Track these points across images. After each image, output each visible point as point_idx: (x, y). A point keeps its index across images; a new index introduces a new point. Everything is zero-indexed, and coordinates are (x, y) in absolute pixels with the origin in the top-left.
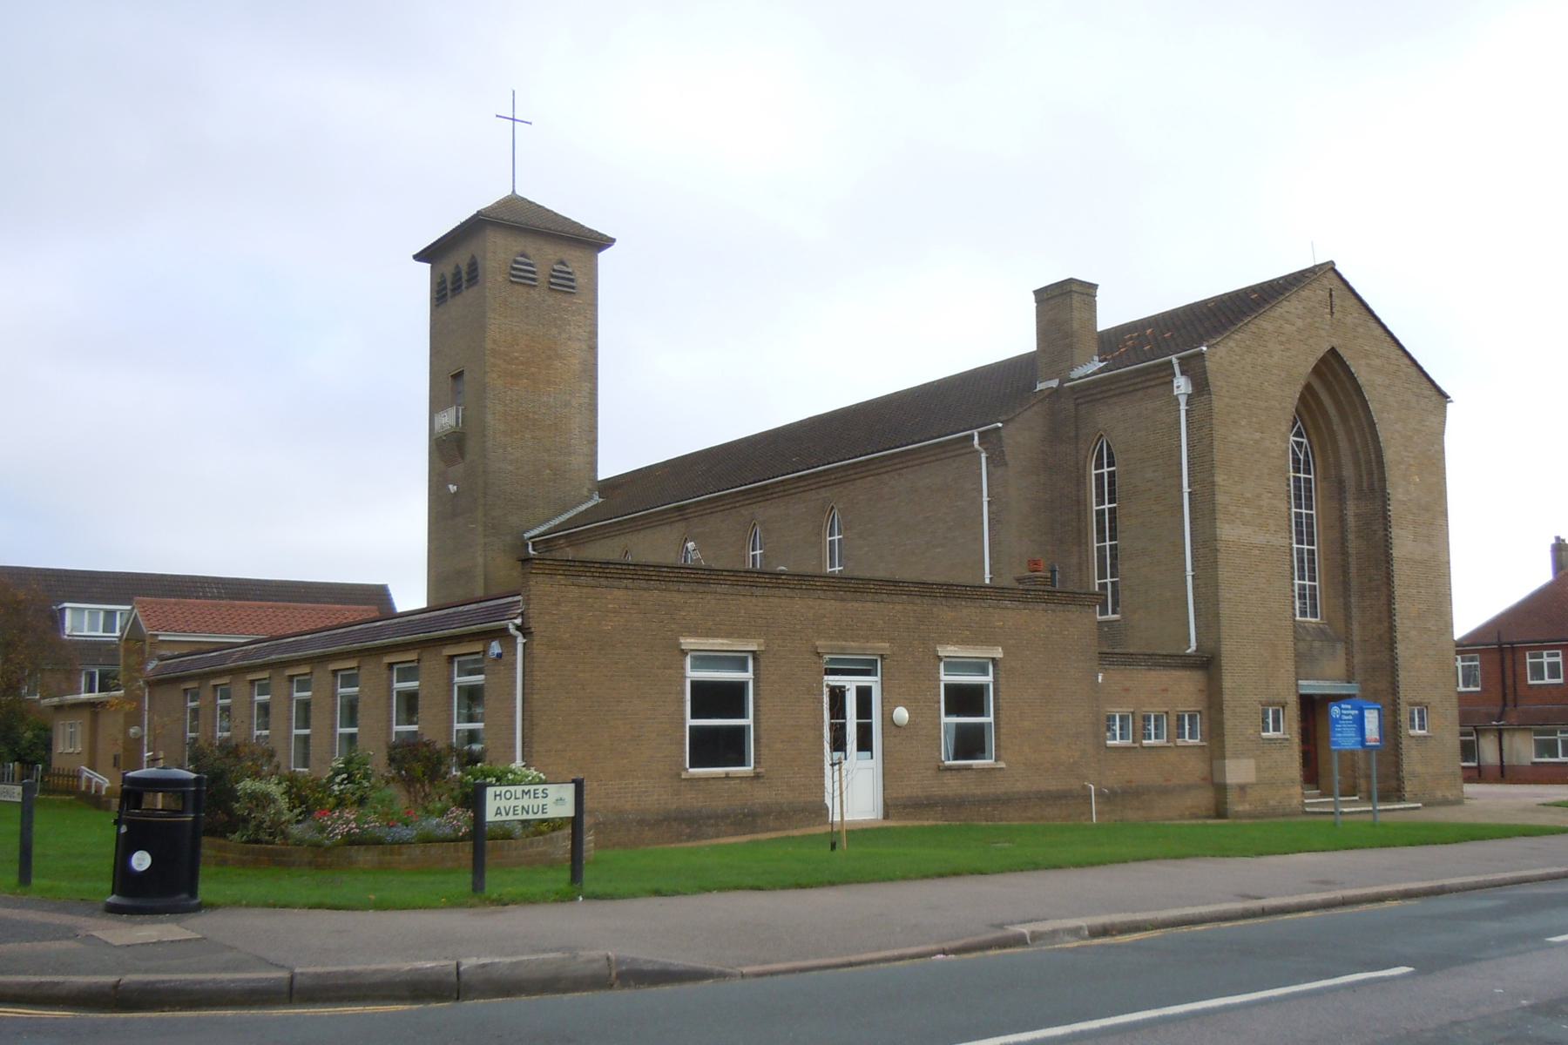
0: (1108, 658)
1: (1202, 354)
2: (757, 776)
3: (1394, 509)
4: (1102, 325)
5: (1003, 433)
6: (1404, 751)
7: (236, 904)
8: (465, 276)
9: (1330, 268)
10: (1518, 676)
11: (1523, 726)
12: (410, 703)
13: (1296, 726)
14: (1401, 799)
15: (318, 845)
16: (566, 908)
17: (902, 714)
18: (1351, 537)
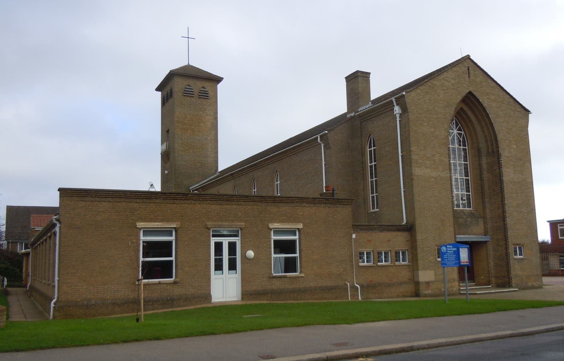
0: (357, 227)
1: (403, 96)
3: (503, 160)
5: (329, 135)
6: (511, 265)
9: (468, 58)
14: (510, 286)
17: (251, 254)
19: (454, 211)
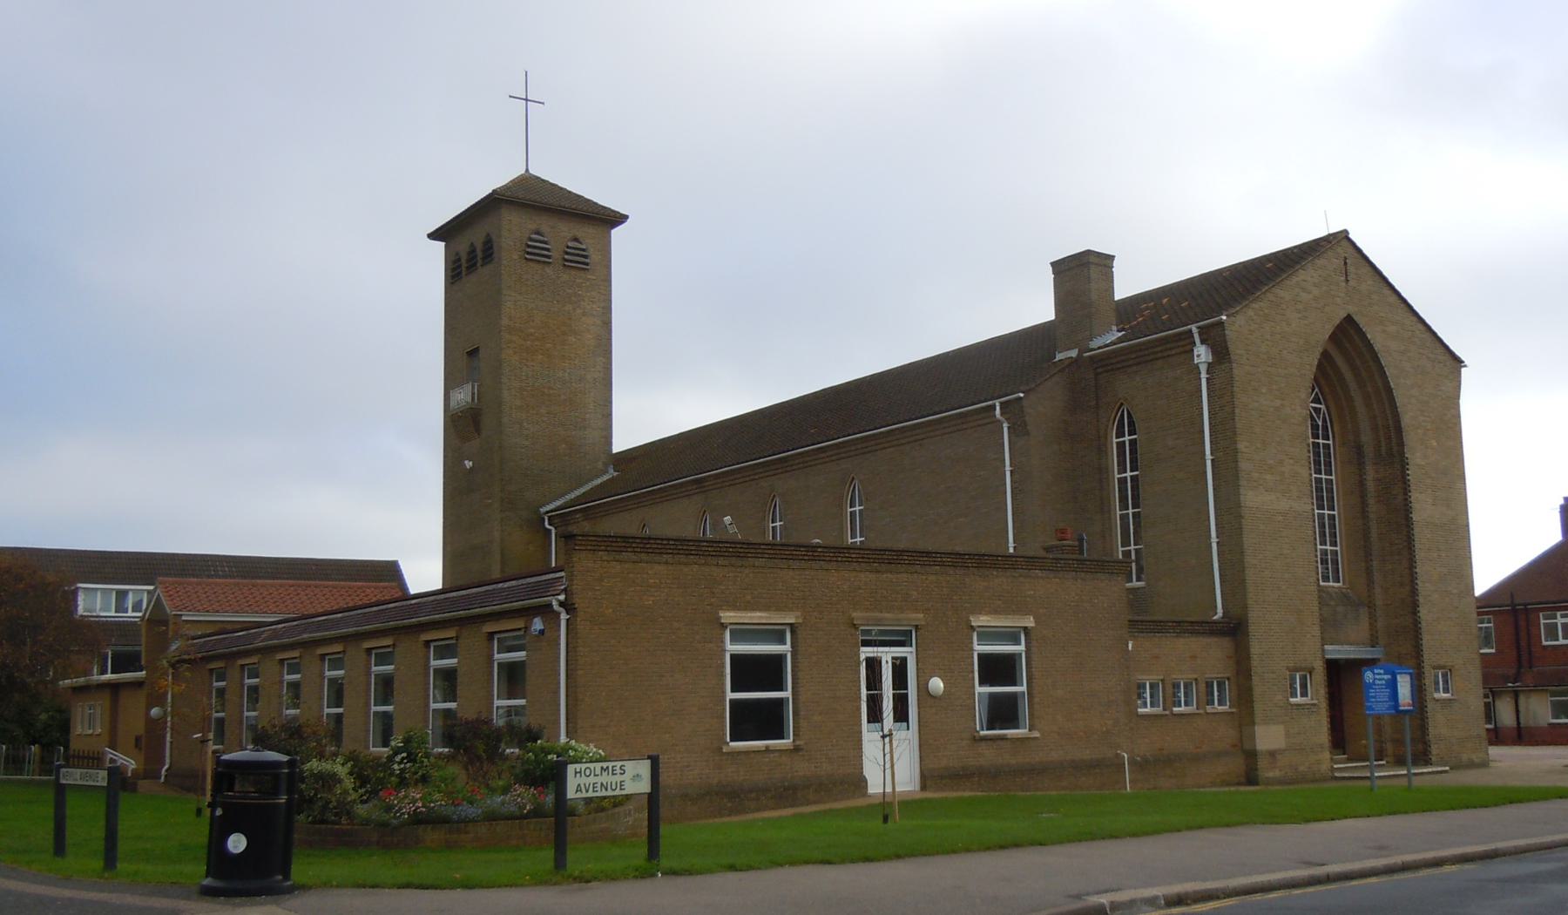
1: (1221, 323)
2: (797, 749)
3: (1412, 474)
4: (1120, 294)
5: (1025, 403)
7: (326, 885)
8: (479, 254)
9: (1343, 236)
10: (1532, 637)
11: (1540, 686)
12: (448, 678)
13: (1323, 691)
14: (1428, 763)
15: (385, 825)
16: (648, 883)
17: (937, 684)
18: (1371, 501)
19: (1321, 589)
